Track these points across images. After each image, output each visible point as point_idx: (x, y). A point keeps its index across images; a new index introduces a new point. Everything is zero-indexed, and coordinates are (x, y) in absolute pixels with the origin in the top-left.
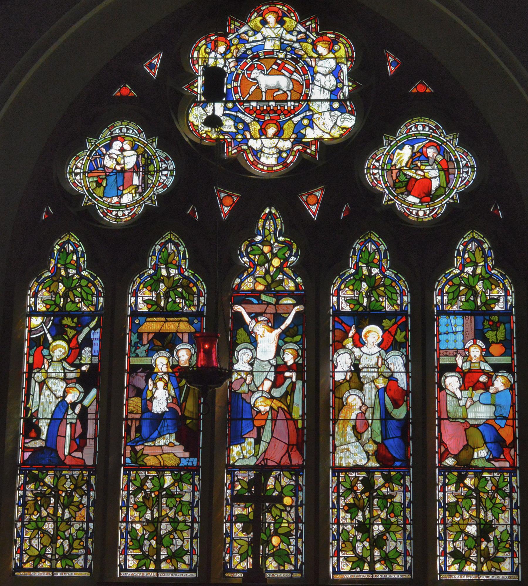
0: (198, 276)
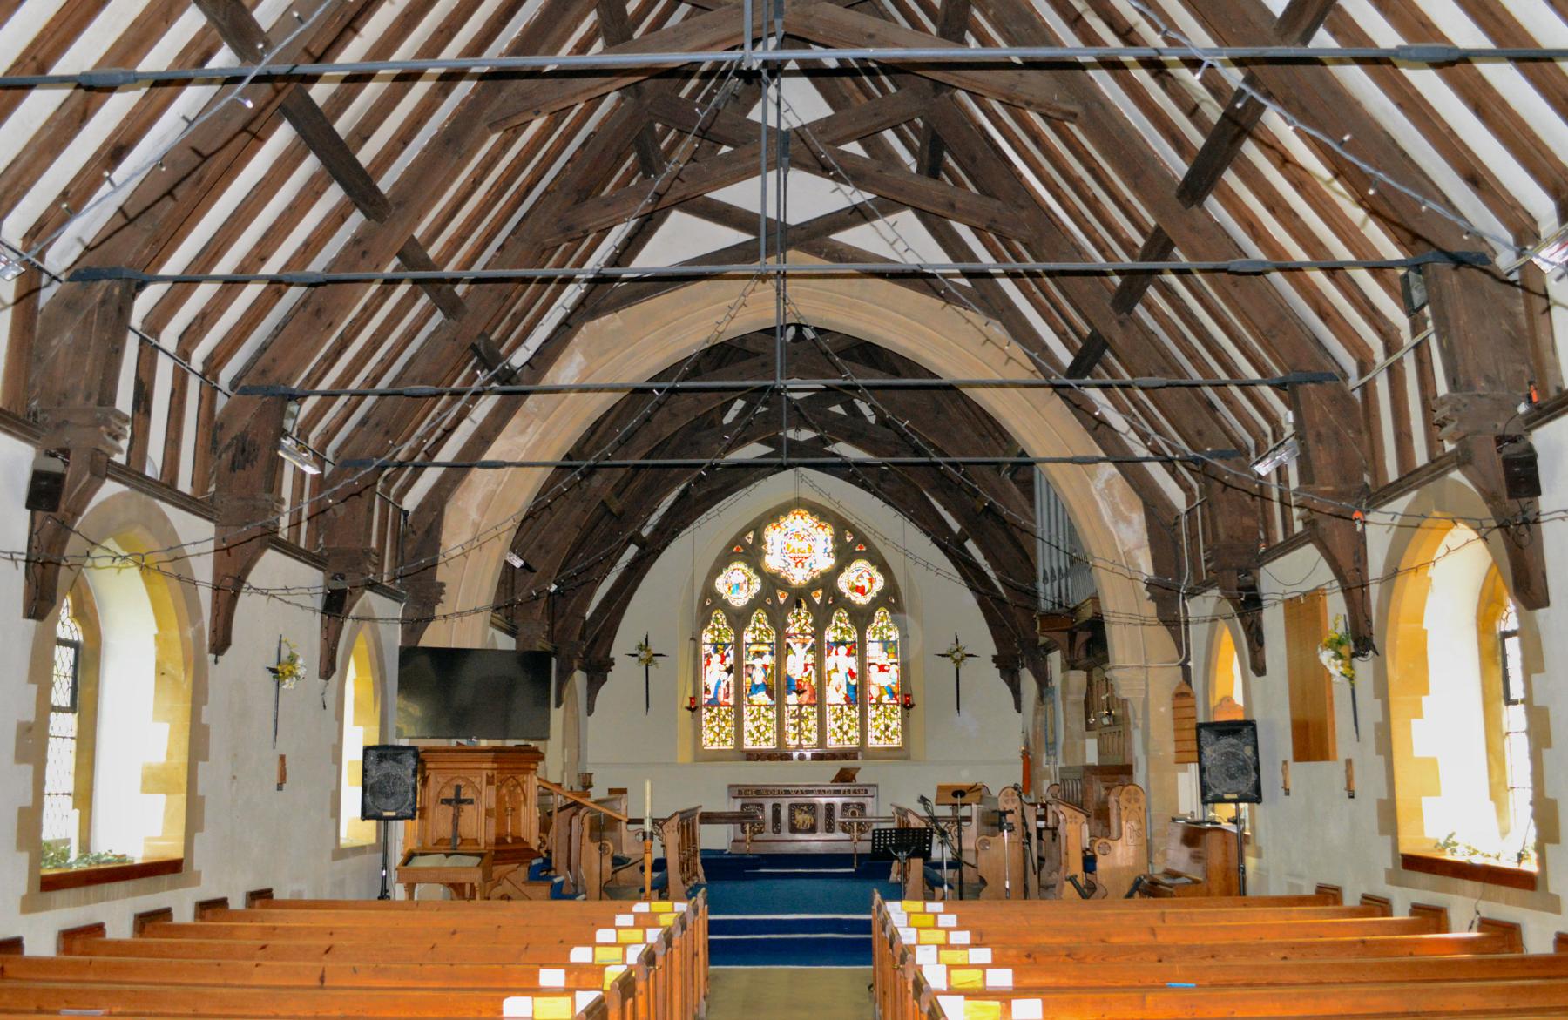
0: (654, 519)
